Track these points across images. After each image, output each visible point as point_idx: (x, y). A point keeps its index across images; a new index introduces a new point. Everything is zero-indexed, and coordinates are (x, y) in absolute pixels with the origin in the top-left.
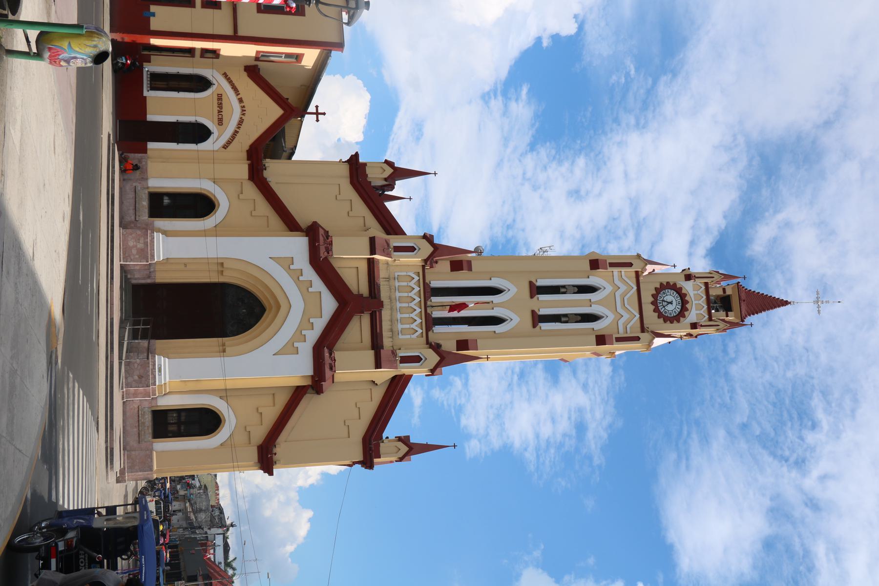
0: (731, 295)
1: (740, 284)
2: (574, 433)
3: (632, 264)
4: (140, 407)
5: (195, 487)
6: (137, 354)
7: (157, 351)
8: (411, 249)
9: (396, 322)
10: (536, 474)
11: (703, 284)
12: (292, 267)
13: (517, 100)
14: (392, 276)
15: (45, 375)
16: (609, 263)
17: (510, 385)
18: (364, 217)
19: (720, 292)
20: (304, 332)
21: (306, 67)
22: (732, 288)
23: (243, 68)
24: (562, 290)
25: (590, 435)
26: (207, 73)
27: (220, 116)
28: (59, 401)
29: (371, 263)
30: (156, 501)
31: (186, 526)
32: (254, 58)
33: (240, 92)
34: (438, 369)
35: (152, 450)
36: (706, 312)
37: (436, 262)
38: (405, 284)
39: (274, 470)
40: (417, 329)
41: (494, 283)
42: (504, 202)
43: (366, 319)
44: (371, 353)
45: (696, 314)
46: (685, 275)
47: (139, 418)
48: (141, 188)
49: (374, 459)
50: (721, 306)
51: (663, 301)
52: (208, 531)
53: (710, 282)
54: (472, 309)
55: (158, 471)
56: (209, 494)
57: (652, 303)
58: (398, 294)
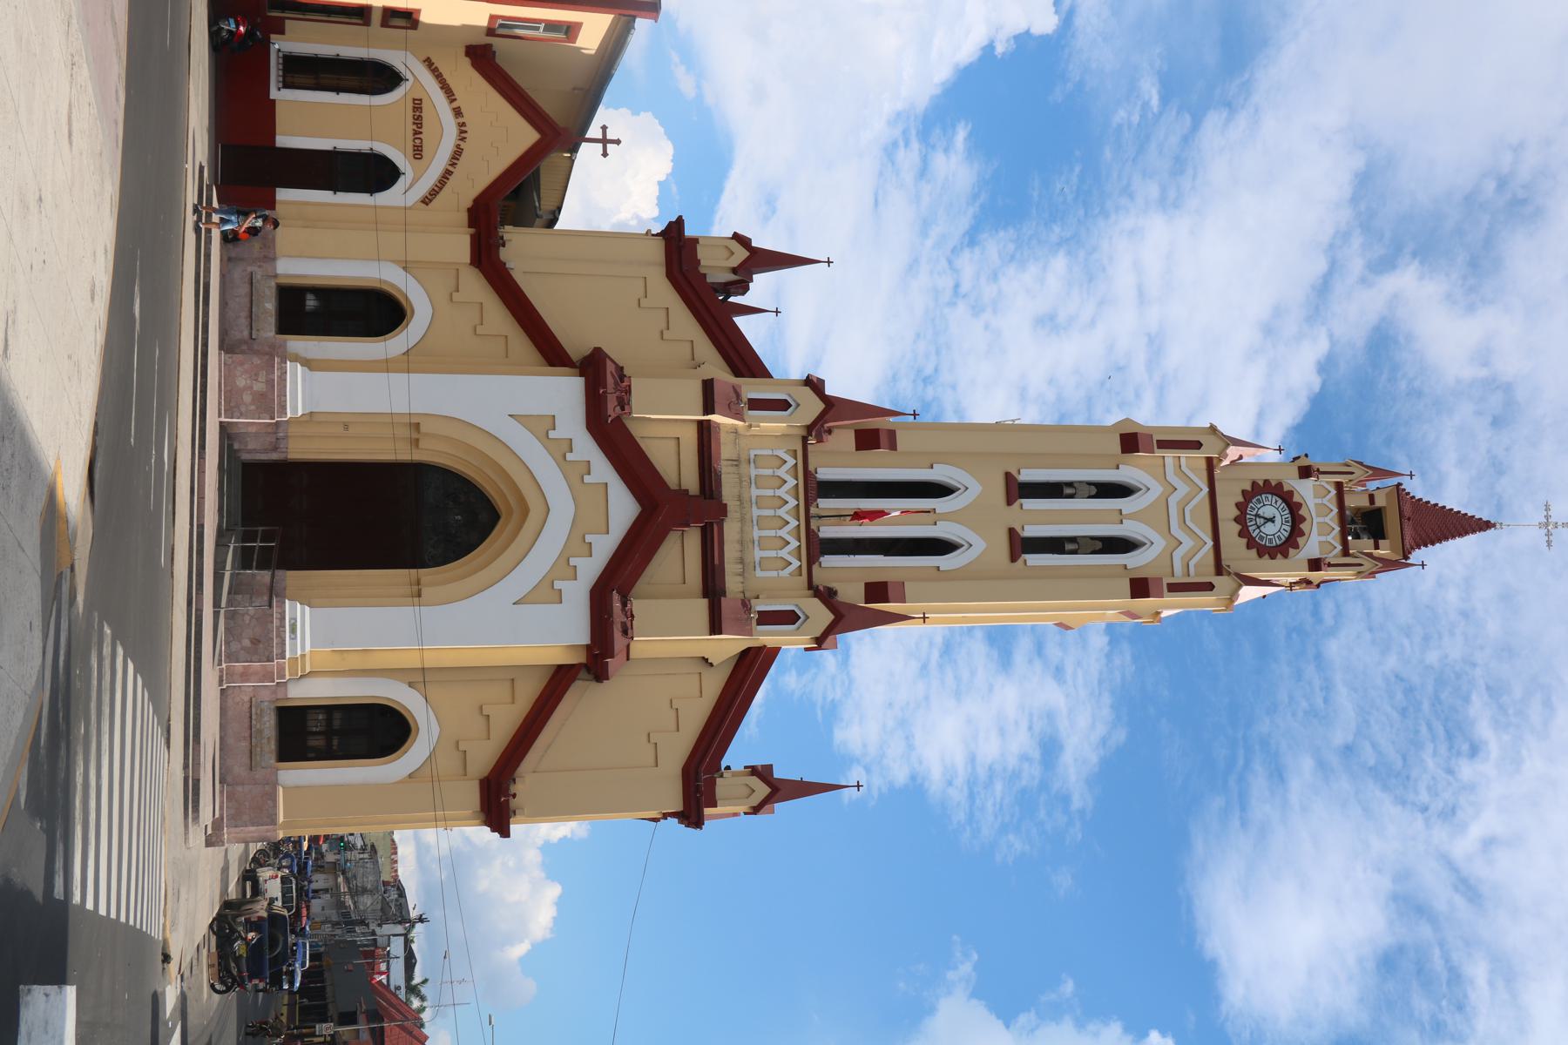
0: (1384, 507)
1: (1402, 487)
2: (1036, 754)
3: (1201, 445)
4: (253, 699)
5: (354, 846)
6: (248, 596)
7: (287, 592)
8: (782, 405)
9: (750, 546)
10: (968, 828)
11: (1333, 485)
12: (552, 434)
13: (946, 150)
14: (744, 457)
15: (38, 623)
16: (1157, 441)
17: (924, 667)
18: (692, 341)
19: (1364, 502)
20: (573, 561)
21: (583, 51)
22: (1387, 494)
23: (464, 49)
24: (1068, 491)
25: (1068, 758)
26: (393, 58)
27: (418, 141)
28: (78, 684)
29: (705, 430)
30: (282, 877)
31: (337, 920)
32: (485, 31)
33: (456, 97)
34: (831, 637)
35: (275, 784)
36: (1338, 538)
37: (830, 431)
38: (769, 472)
39: (511, 826)
40: (790, 559)
41: (938, 474)
42: (918, 335)
43: (693, 538)
44: (702, 605)
45: (1320, 542)
46: (1299, 467)
47: (251, 722)
48: (262, 276)
49: (705, 809)
50: (1365, 529)
51: (1257, 515)
52: (378, 930)
53: (1347, 483)
54: (895, 522)
55: (286, 825)
56: (379, 860)
57: (1237, 520)
58: (755, 492)
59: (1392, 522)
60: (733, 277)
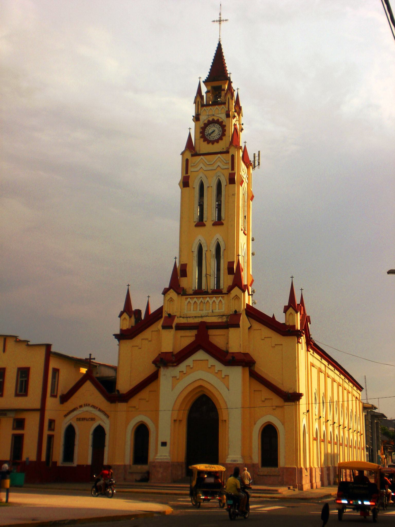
27: (89, 420)
43: (211, 332)
59: (216, 84)
60: (133, 317)
